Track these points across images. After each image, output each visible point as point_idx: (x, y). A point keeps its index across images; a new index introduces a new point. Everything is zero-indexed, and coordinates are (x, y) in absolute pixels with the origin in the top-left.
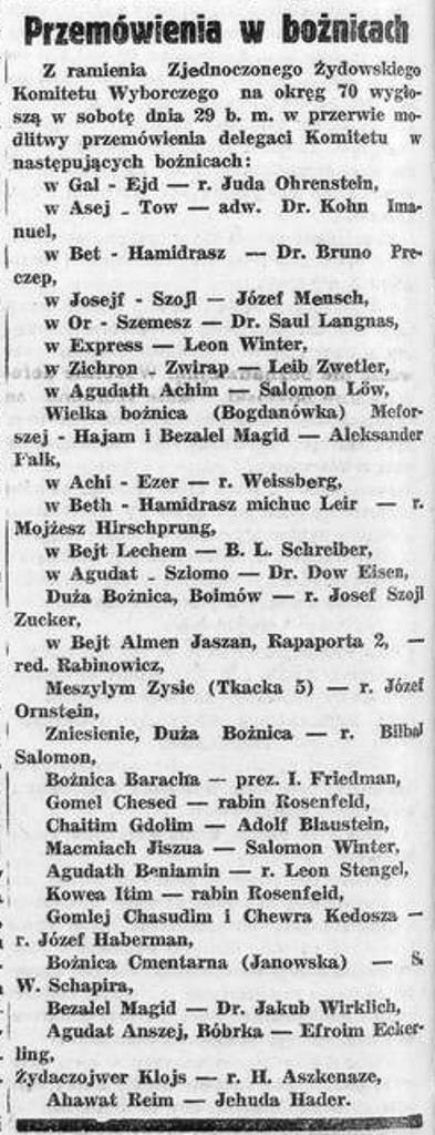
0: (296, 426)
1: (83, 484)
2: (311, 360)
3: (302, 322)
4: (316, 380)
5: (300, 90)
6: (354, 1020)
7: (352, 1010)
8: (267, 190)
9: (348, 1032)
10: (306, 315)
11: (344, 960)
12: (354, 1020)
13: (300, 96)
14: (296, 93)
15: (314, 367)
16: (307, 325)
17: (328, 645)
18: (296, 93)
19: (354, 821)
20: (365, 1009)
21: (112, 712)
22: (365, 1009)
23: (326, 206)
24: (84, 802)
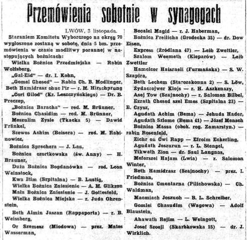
0: (100, 92)
1: (36, 133)
2: (146, 80)
3: (23, 95)
4: (147, 174)
5: (109, 37)
6: (203, 35)
7: (183, 227)
8: (226, 103)
9: (202, 220)
10: (198, 151)
11: (221, 184)
12: (203, 35)
13: (108, 38)
14: (107, 37)
15: (169, 139)
16: (198, 153)
17: (197, 171)
18: (107, 37)
19: (142, 211)
20: (140, 233)
21: (30, 127)
22: (140, 233)
23: (42, 120)
24: (151, 115)
